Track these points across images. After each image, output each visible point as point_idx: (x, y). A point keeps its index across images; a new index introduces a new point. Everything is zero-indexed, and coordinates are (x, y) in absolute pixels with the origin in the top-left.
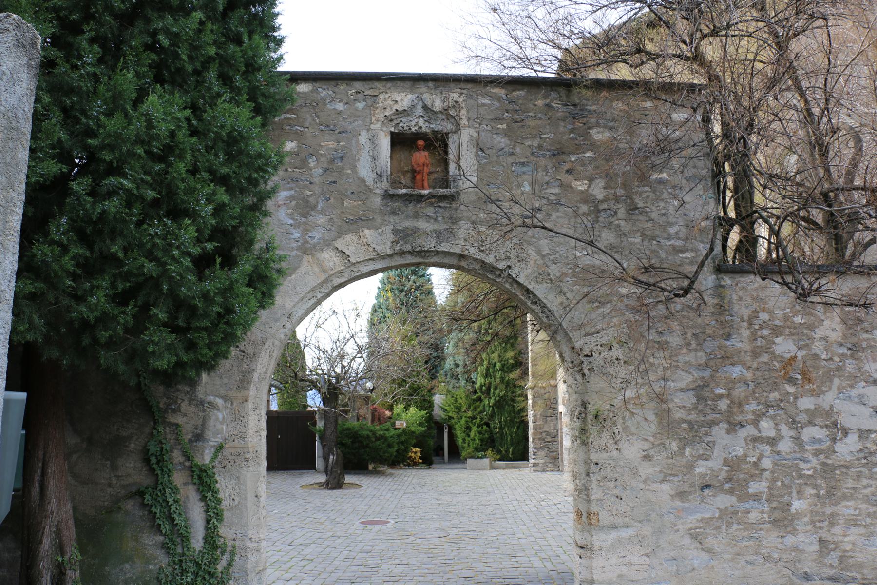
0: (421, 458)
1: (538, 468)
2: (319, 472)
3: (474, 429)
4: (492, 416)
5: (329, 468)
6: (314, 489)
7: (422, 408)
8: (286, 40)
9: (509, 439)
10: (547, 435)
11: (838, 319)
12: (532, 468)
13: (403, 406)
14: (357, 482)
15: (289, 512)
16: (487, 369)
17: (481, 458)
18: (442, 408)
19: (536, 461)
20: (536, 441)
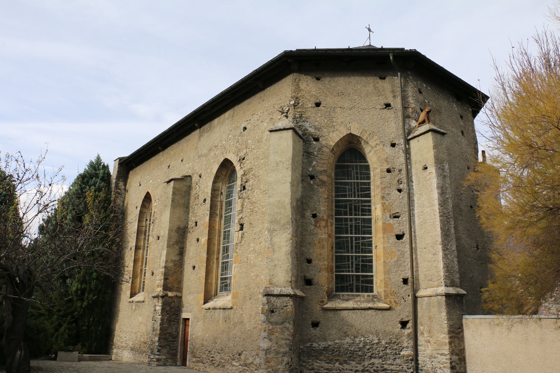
1: (161, 363)
8: (101, 156)
9: (93, 336)
10: (169, 336)
11: (372, 87)
16: (84, 276)
17: (72, 351)
19: (160, 357)
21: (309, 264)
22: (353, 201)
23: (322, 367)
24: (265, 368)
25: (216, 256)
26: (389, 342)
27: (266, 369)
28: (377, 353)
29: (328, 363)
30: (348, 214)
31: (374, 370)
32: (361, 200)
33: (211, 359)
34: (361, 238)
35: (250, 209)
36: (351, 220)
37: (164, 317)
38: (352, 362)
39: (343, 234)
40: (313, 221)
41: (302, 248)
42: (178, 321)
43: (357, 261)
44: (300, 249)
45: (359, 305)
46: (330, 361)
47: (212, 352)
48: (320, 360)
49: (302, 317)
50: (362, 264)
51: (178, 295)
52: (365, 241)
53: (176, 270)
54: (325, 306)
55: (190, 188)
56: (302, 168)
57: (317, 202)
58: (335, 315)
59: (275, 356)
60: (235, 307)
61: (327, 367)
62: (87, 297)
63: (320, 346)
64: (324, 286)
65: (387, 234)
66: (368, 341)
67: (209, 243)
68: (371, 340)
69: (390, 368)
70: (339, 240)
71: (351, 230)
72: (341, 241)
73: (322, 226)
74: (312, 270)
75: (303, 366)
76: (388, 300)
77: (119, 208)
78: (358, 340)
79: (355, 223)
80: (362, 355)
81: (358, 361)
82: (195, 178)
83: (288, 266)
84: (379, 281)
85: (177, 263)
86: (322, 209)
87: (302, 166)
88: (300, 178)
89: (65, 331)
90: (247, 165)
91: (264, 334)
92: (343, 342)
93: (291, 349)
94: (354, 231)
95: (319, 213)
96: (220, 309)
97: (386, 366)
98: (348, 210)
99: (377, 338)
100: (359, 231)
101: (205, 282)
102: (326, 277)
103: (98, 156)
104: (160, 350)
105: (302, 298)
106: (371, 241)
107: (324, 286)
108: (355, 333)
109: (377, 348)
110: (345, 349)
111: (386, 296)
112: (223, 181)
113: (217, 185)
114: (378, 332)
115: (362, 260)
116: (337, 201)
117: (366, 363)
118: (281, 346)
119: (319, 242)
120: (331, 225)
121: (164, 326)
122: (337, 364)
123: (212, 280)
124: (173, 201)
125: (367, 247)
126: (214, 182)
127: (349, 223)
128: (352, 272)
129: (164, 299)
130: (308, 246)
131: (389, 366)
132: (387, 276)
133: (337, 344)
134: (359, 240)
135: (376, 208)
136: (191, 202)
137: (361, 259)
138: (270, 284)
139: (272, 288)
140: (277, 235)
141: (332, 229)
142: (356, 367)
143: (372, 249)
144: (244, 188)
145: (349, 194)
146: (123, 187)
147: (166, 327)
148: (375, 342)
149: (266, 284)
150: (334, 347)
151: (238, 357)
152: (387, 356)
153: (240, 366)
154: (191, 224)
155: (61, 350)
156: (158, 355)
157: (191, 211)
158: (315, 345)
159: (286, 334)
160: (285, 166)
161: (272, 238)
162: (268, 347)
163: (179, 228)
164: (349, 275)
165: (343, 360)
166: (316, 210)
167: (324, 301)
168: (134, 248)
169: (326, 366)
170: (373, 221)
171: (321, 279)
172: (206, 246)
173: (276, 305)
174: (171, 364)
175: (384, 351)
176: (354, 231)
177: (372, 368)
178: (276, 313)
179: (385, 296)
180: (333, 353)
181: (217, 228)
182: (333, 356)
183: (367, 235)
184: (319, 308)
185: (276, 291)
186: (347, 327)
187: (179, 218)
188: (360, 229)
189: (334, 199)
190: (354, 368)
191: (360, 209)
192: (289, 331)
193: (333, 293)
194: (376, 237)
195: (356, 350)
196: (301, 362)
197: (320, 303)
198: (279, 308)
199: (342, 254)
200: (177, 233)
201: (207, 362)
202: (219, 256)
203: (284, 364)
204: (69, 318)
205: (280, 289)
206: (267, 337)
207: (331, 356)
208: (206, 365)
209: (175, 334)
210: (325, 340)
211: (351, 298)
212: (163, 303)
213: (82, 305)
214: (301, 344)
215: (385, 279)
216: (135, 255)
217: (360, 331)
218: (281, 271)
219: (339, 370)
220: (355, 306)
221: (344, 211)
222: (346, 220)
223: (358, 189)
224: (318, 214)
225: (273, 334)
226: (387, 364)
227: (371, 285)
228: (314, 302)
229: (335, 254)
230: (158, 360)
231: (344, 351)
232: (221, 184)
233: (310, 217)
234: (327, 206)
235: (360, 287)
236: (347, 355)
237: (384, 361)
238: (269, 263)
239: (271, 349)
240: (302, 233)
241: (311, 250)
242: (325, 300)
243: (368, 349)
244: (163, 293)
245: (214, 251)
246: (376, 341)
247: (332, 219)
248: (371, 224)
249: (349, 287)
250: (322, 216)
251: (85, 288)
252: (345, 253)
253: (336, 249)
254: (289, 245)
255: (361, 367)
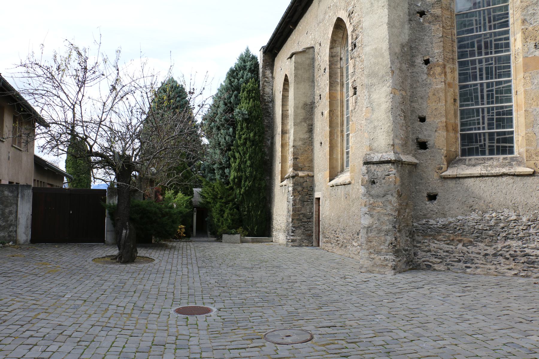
0: (184, 233)
1: (296, 244)
2: (108, 245)
3: (227, 211)
4: (242, 202)
5: (122, 242)
6: (107, 262)
7: (186, 194)
8: (250, 49)
9: (254, 220)
12: (291, 244)
13: (173, 191)
14: (147, 255)
15: (85, 296)
16: (239, 165)
17: (234, 234)
18: (201, 195)
19: (295, 238)
20: (295, 221)
21: (422, 123)
22: (483, 35)
23: (441, 249)
24: (366, 248)
25: (340, 129)
26: (533, 218)
27: (368, 250)
28: (515, 233)
29: (448, 244)
30: (476, 54)
31: (510, 254)
32: (495, 33)
33: (336, 239)
34: (494, 83)
35: (361, 69)
36: (480, 61)
37: (296, 197)
38: (479, 244)
39: (470, 81)
40: (425, 68)
41: (413, 104)
42: (312, 201)
43: (491, 114)
44: (411, 106)
45: (489, 171)
46: (451, 242)
47: (337, 232)
48: (438, 241)
49: (416, 189)
50: (496, 118)
51: (310, 174)
52: (501, 86)
53: (306, 149)
54: (443, 174)
55: (313, 59)
56: (409, 4)
57: (429, 44)
58: (457, 185)
59: (377, 235)
60: (353, 182)
61: (448, 249)
62: (244, 184)
63: (438, 224)
64: (443, 149)
65: (530, 72)
66: (502, 218)
67: (331, 115)
68: (506, 216)
69: (534, 253)
70: (465, 89)
71: (481, 75)
72: (467, 90)
73: (437, 73)
74: (426, 130)
75: (417, 247)
76: (532, 162)
77: (269, 97)
78: (488, 216)
79: (486, 65)
80: (494, 235)
81: (488, 243)
82: (317, 48)
83: (389, 126)
84: (520, 138)
85: (306, 141)
86: (436, 51)
87: (408, 2)
88: (407, 18)
89: (228, 216)
90: (356, 18)
91: (365, 209)
92: (467, 218)
93: (394, 227)
94: (484, 76)
95: (433, 57)
96: (341, 185)
97: (527, 251)
98: (476, 48)
99: (515, 214)
100: (492, 75)
101: (330, 158)
102: (444, 137)
103: (248, 48)
104: (294, 230)
105: (415, 165)
106: (510, 86)
107: (443, 149)
108: (484, 207)
109: (515, 226)
110: (470, 227)
111: (529, 158)
112: (341, 44)
113: (334, 50)
114: (516, 205)
115: (496, 112)
116: (460, 40)
117: (499, 246)
118: (383, 223)
119: (434, 94)
120: (452, 71)
121: (297, 206)
122: (460, 246)
123: (337, 155)
124: (295, 76)
125: (504, 95)
126: (331, 48)
127: (478, 66)
128: (484, 128)
129: (294, 179)
130: (420, 101)
131: (533, 250)
132: (530, 130)
133: (460, 221)
134: (492, 86)
135: (515, 40)
136: (315, 74)
137: (495, 111)
138: (371, 150)
139: (372, 155)
140: (375, 90)
141: (454, 76)
142: (484, 250)
143: (511, 96)
144: (355, 46)
145: (477, 28)
146: (271, 75)
147: (298, 208)
148: (511, 218)
149: (365, 150)
150: (456, 225)
151: (357, 236)
152: (531, 237)
153: (358, 247)
154: (317, 98)
155: (225, 234)
156: (292, 236)
157: (316, 84)
158: (432, 222)
159: (388, 209)
160: (380, 5)
161: (370, 95)
162: (370, 224)
163: (305, 104)
164: (480, 134)
165: (468, 241)
166: (429, 55)
167: (442, 168)
168: (280, 133)
169: (446, 247)
170: (512, 58)
171: (439, 140)
172: (328, 119)
173: (377, 174)
174: (307, 244)
175: (525, 231)
176: (484, 76)
177: (507, 251)
178: (377, 184)
179: (527, 157)
180: (455, 233)
181: (339, 98)
182: (455, 236)
183: (503, 78)
184: (436, 176)
185: (376, 158)
186: (473, 199)
187: (304, 93)
188: (494, 72)
189: (455, 38)
190: (482, 251)
191: (493, 46)
192: (392, 205)
193: (457, 158)
194: (516, 80)
195: (485, 229)
196: (415, 242)
197: (437, 171)
198: (380, 178)
199: (469, 107)
200: (304, 109)
201: (334, 242)
202: (343, 128)
203: (387, 245)
204: (231, 204)
205: (380, 155)
206: (368, 213)
207: (452, 235)
208: (333, 246)
209: (310, 215)
210: (444, 215)
211: (481, 162)
212: (294, 183)
213: (240, 192)
214: (415, 221)
215: (526, 134)
216: (282, 140)
217: (491, 205)
218: (382, 133)
219: (462, 252)
220: (484, 172)
221: (470, 51)
222: (473, 62)
223: (490, 18)
224: (431, 59)
225: (374, 209)
226: (530, 247)
227: (511, 145)
228: (430, 169)
229: (459, 108)
230: (293, 241)
231: (469, 230)
232: (339, 48)
233: (421, 65)
234: (443, 47)
235: (495, 148)
236: (473, 235)
237: (525, 244)
238: (368, 125)
239: (372, 226)
240: (411, 86)
241: (424, 106)
242: (444, 167)
243: (503, 228)
244: (293, 173)
245: (337, 124)
246: (514, 217)
247: (453, 63)
248: (510, 63)
249: (480, 149)
250: (436, 60)
251: (241, 176)
252: (472, 105)
253: (461, 102)
254: (390, 101)
255: (493, 251)
